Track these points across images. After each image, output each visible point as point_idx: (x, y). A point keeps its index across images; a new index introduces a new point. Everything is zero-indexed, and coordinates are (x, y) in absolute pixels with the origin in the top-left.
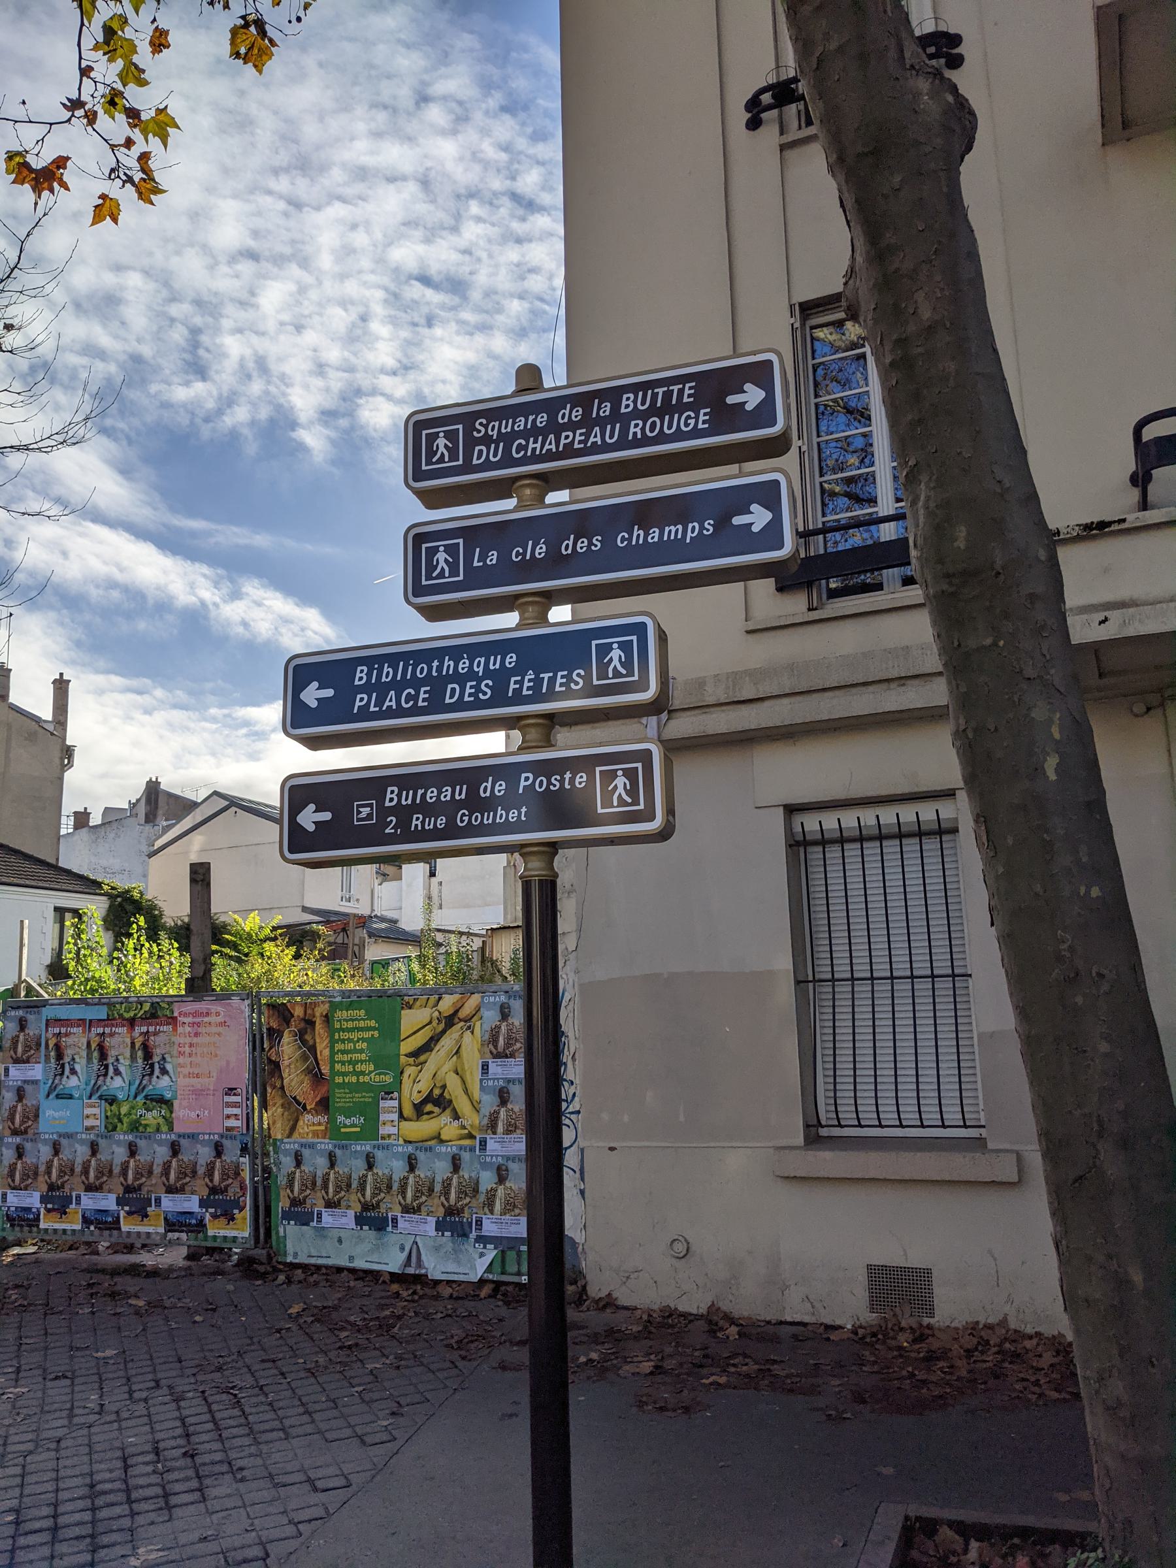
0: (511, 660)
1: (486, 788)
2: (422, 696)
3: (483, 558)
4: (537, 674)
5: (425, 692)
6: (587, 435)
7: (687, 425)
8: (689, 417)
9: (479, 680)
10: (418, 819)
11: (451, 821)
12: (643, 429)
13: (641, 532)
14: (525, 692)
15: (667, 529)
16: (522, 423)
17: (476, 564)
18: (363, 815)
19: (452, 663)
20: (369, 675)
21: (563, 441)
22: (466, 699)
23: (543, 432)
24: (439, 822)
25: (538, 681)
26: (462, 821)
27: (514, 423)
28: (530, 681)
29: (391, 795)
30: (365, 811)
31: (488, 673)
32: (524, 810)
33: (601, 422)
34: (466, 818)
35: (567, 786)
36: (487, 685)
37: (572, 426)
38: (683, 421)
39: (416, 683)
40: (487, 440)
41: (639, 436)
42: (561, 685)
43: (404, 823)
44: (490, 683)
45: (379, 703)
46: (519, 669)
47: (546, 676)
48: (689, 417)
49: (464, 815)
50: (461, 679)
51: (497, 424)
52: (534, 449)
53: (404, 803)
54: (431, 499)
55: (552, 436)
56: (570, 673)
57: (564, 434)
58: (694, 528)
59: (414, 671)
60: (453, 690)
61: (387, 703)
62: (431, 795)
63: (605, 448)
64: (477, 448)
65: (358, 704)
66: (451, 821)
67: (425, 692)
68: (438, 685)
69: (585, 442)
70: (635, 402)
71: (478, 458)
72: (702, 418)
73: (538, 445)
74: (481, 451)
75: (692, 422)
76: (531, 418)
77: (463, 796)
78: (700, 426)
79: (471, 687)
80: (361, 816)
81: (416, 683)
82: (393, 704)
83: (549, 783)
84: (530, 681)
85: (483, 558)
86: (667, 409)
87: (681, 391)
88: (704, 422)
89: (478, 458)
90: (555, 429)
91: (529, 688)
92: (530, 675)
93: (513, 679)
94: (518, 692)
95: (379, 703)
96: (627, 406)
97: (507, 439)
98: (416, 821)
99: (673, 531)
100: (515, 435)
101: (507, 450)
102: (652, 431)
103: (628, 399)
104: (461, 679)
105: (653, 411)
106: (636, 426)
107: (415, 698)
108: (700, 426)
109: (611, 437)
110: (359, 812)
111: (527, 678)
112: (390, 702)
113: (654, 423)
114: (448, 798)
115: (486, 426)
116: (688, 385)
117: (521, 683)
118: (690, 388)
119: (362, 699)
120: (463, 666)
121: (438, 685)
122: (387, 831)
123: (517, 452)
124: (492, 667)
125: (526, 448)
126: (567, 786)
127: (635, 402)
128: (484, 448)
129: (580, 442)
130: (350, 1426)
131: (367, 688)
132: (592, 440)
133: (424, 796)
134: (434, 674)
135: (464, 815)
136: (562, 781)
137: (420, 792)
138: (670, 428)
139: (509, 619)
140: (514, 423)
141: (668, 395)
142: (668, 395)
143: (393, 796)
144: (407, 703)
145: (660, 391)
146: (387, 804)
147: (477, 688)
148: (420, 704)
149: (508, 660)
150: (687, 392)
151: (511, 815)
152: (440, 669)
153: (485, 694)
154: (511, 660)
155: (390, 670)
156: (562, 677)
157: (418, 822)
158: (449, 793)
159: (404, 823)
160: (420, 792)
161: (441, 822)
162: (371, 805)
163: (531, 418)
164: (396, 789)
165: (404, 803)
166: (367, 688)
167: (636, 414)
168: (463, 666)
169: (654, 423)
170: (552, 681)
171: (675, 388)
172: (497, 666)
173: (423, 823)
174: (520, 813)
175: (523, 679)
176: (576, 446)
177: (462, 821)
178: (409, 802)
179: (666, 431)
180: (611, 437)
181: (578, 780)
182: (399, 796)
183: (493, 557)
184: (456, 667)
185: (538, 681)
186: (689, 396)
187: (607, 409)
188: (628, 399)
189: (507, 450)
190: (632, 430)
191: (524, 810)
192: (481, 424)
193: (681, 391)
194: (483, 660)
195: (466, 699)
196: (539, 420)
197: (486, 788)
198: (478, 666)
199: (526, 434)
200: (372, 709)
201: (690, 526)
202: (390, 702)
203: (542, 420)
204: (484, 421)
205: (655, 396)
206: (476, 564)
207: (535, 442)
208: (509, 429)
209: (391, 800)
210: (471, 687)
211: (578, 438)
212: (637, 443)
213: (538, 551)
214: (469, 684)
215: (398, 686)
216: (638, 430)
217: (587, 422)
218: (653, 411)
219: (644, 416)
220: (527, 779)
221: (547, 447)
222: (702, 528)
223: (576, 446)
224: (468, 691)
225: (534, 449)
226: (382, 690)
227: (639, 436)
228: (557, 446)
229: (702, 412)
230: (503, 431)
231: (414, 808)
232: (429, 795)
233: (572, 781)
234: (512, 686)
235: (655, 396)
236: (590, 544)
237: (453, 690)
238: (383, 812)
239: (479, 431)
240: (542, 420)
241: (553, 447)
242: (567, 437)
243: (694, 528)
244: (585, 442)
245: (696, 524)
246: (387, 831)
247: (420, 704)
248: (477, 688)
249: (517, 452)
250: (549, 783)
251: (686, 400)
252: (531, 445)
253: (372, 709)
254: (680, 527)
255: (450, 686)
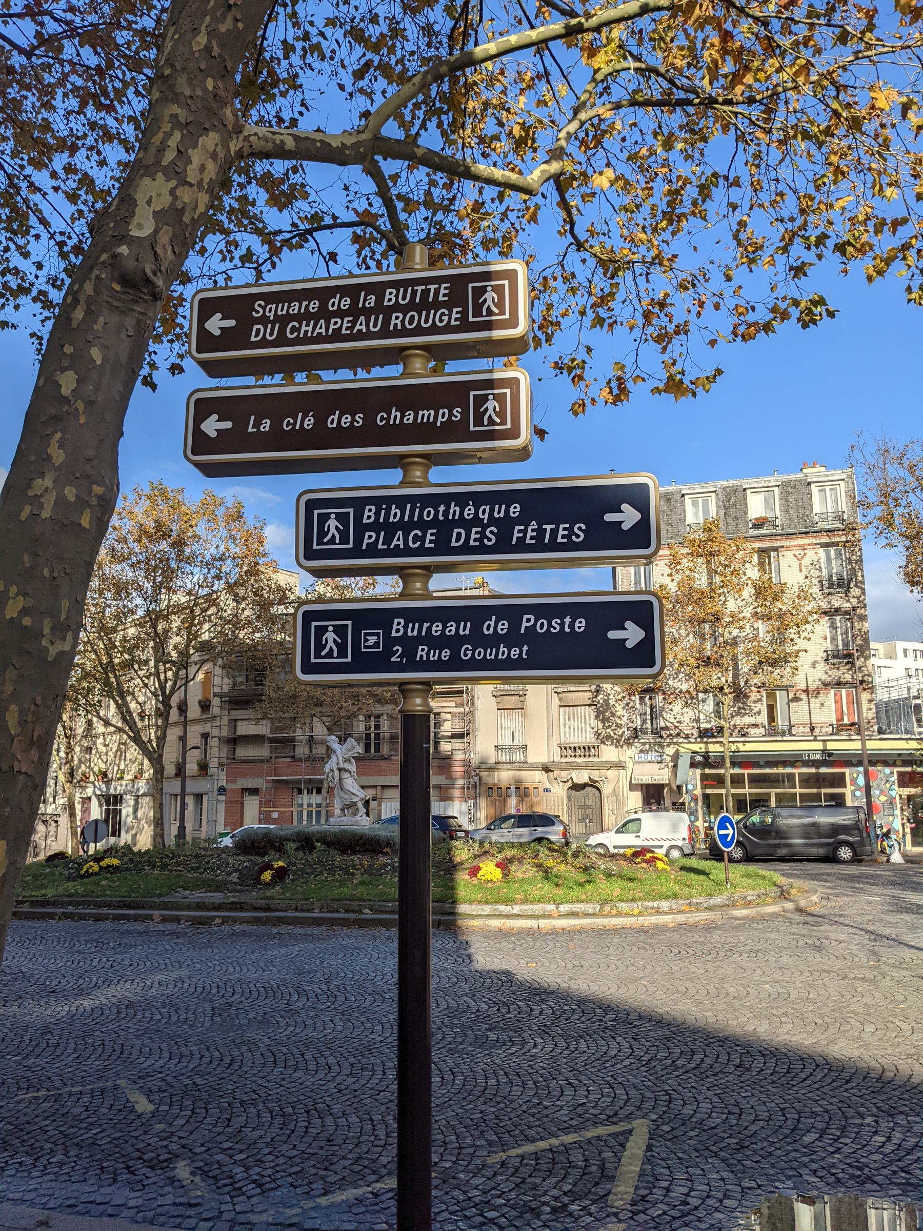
0: (515, 510)
1: (489, 626)
2: (429, 538)
3: (257, 425)
4: (540, 525)
5: (432, 534)
6: (354, 323)
7: (441, 321)
8: (443, 314)
9: (485, 527)
10: (423, 650)
11: (455, 654)
12: (403, 322)
13: (398, 414)
14: (528, 541)
15: (421, 413)
16: (297, 308)
17: (250, 430)
18: (370, 643)
19: (457, 509)
20: (377, 514)
21: (332, 327)
22: (472, 543)
23: (316, 317)
24: (443, 654)
25: (541, 532)
26: (466, 655)
27: (289, 307)
28: (533, 530)
29: (398, 625)
30: (372, 640)
31: (492, 521)
32: (525, 648)
33: (367, 312)
34: (470, 653)
35: (567, 630)
36: (491, 532)
37: (340, 314)
38: (439, 317)
39: (423, 525)
40: (264, 320)
41: (399, 327)
42: (475, 540)
43: (409, 652)
44: (495, 530)
45: (387, 541)
46: (524, 519)
47: (549, 527)
48: (443, 314)
49: (467, 649)
50: (467, 525)
51: (274, 306)
52: (306, 332)
53: (410, 634)
54: (212, 369)
55: (322, 321)
56: (572, 527)
57: (333, 320)
58: (444, 414)
59: (421, 514)
60: (459, 534)
61: (395, 542)
62: (437, 628)
63: (368, 335)
64: (255, 327)
65: (366, 541)
66: (455, 654)
67: (432, 534)
68: (444, 528)
69: (351, 328)
70: (397, 296)
71: (256, 336)
72: (454, 316)
73: (310, 329)
74: (258, 330)
75: (446, 318)
76: (305, 303)
77: (467, 632)
78: (453, 323)
79: (477, 533)
80: (367, 644)
81: (423, 525)
82: (401, 543)
83: (550, 625)
84: (533, 530)
85: (257, 425)
86: (425, 305)
87: (437, 291)
88: (456, 319)
89: (256, 336)
90: (324, 314)
91: (532, 538)
92: (533, 525)
93: (517, 528)
94: (521, 540)
95: (387, 541)
96: (390, 300)
97: (283, 320)
98: (422, 652)
99: (426, 415)
100: (289, 318)
101: (282, 331)
102: (410, 324)
103: (391, 293)
104: (467, 525)
105: (412, 306)
106: (397, 318)
107: (423, 539)
108: (453, 323)
109: (375, 326)
110: (366, 640)
111: (530, 528)
112: (398, 541)
113: (412, 317)
114: (453, 633)
115: (264, 308)
116: (443, 286)
117: (525, 532)
118: (445, 288)
119: (370, 537)
120: (469, 512)
121: (444, 528)
122: (393, 659)
123: (291, 333)
124: (496, 515)
125: (298, 330)
126: (567, 630)
127: (397, 296)
128: (261, 327)
129: (347, 328)
130: (653, 1219)
131: (376, 527)
132: (358, 327)
133: (429, 629)
134: (441, 518)
135: (467, 649)
136: (562, 625)
137: (426, 625)
138: (426, 322)
139: (394, 476)
140: (289, 307)
141: (426, 293)
142: (426, 293)
143: (400, 627)
144: (414, 543)
145: (419, 289)
146: (394, 634)
147: (483, 534)
148: (427, 545)
149: (512, 510)
150: (442, 291)
151: (512, 653)
152: (446, 513)
153: (578, 536)
154: (515, 510)
155: (398, 511)
156: (564, 529)
157: (424, 654)
158: (454, 628)
159: (409, 652)
160: (426, 625)
161: (446, 654)
162: (378, 635)
163: (305, 303)
164: (402, 621)
165: (410, 634)
166: (376, 527)
167: (397, 307)
168: (469, 512)
169: (412, 317)
170: (554, 532)
171: (433, 287)
172: (502, 515)
173: (428, 654)
174: (521, 651)
175: (526, 529)
176: (344, 332)
177: (466, 655)
178: (415, 633)
179: (268, 337)
180: (375, 326)
181: (577, 624)
182: (405, 627)
183: (266, 425)
184: (462, 513)
185: (541, 532)
186: (444, 295)
187: (372, 301)
188: (391, 293)
189: (282, 331)
190: (393, 321)
191: (525, 648)
192: (259, 305)
193: (437, 291)
194: (488, 508)
195: (472, 543)
196: (311, 305)
197: (489, 626)
198: (396, 514)
199: (299, 317)
200: (380, 546)
201: (441, 411)
202: (398, 541)
203: (314, 306)
204: (263, 303)
205: (414, 293)
206: (250, 430)
207: (308, 325)
208: (284, 312)
209: (398, 631)
210: (477, 533)
211: (345, 325)
212: (396, 333)
213: (306, 422)
214: (474, 530)
215: (406, 527)
216: (398, 322)
217: (355, 312)
218: (412, 306)
219: (404, 309)
220: (528, 620)
221: (318, 330)
222: (451, 414)
223: (344, 332)
224: (473, 536)
225: (306, 332)
226: (390, 530)
227: (399, 327)
228: (327, 331)
229: (455, 310)
230: (279, 313)
231: (419, 640)
232: (434, 628)
233: (572, 625)
234: (516, 535)
235: (414, 293)
236: (353, 420)
237: (459, 534)
238: (390, 642)
239: (258, 312)
240: (314, 306)
241: (323, 331)
242: (336, 323)
243: (444, 414)
244: (351, 328)
245: (446, 411)
246: (393, 659)
247: (427, 545)
248: (483, 534)
249: (291, 333)
250: (550, 625)
251: (441, 298)
252: (304, 328)
253: (380, 546)
254: (432, 412)
255: (456, 531)
